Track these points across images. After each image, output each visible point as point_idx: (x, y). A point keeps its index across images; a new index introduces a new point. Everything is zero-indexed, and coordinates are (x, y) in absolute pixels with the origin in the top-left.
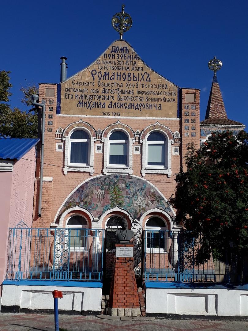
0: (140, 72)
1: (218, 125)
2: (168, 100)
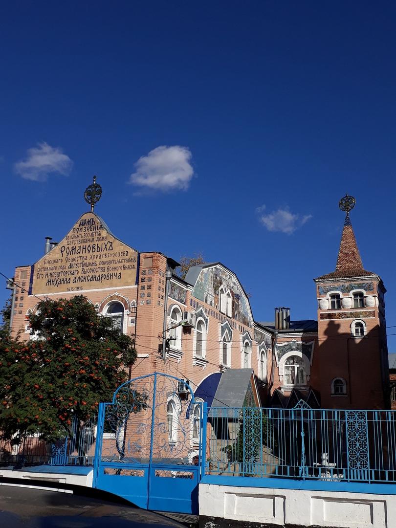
0: (103, 242)
1: (340, 279)
2: (128, 268)
